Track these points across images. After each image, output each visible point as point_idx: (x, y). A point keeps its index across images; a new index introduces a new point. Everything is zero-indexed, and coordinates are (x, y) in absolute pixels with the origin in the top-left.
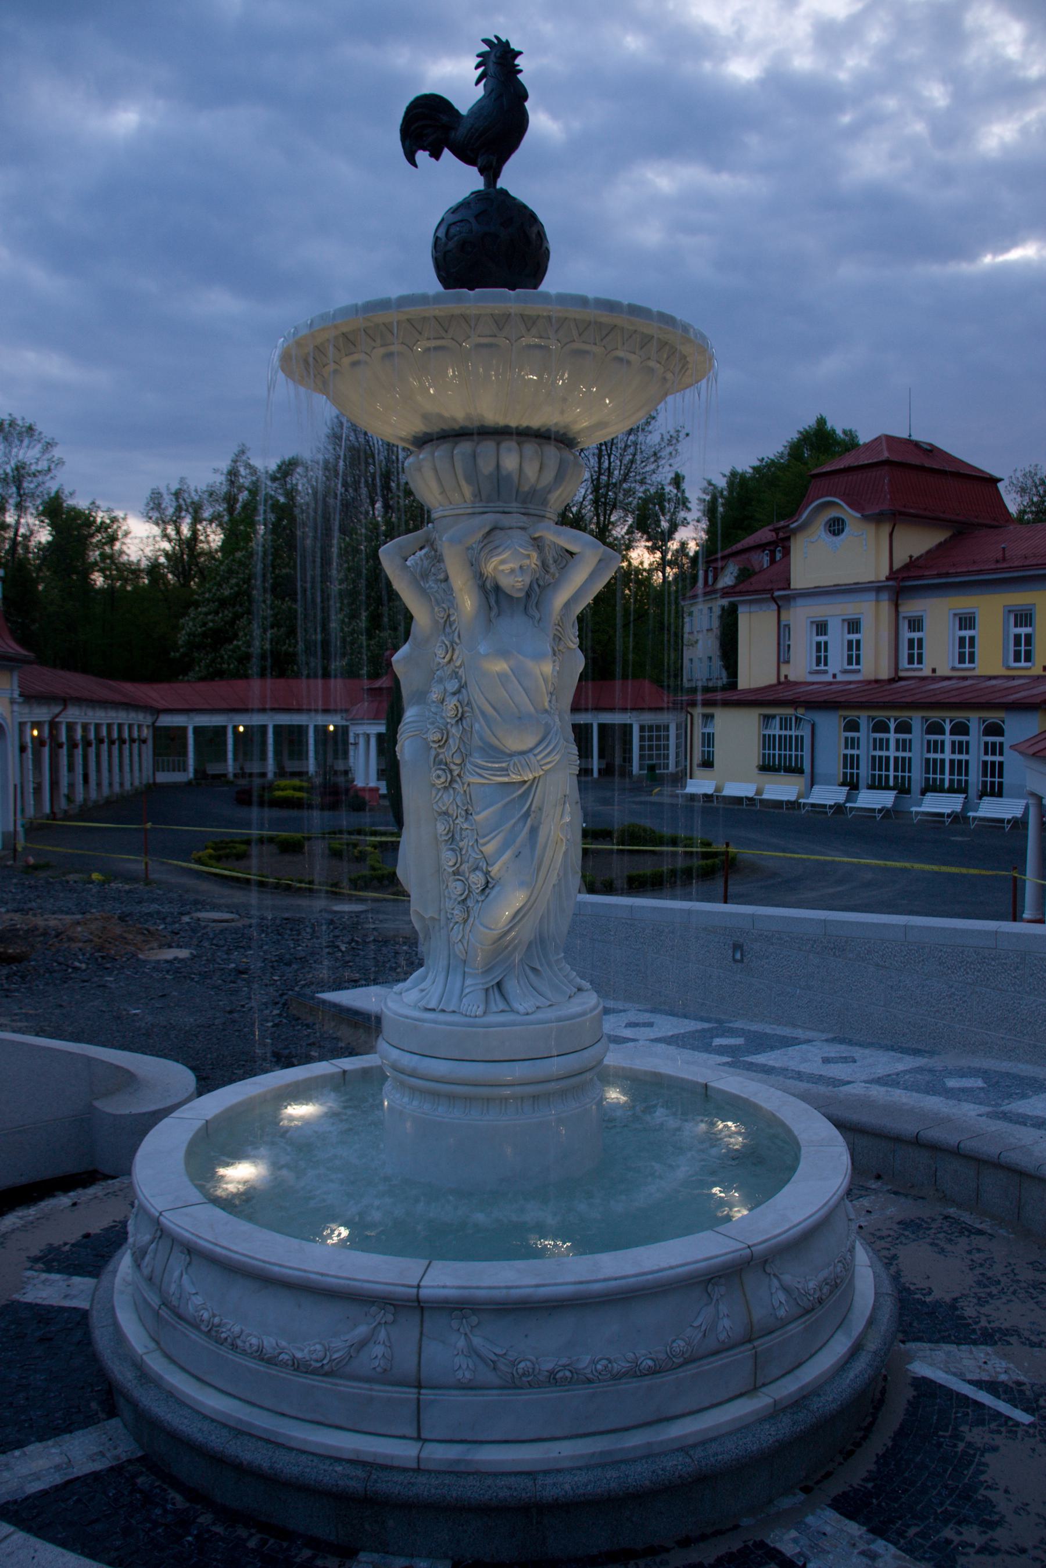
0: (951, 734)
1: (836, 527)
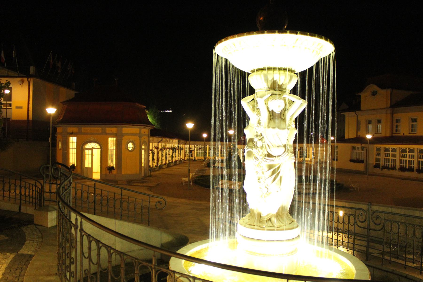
0: (392, 151)
1: (374, 93)
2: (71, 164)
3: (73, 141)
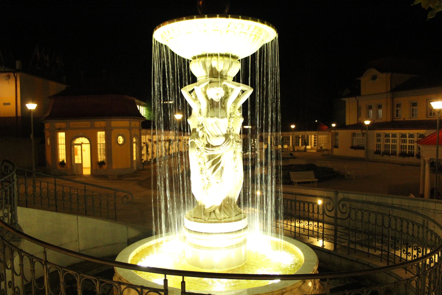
0: (409, 137)
1: (374, 78)
2: (61, 161)
3: (62, 136)
